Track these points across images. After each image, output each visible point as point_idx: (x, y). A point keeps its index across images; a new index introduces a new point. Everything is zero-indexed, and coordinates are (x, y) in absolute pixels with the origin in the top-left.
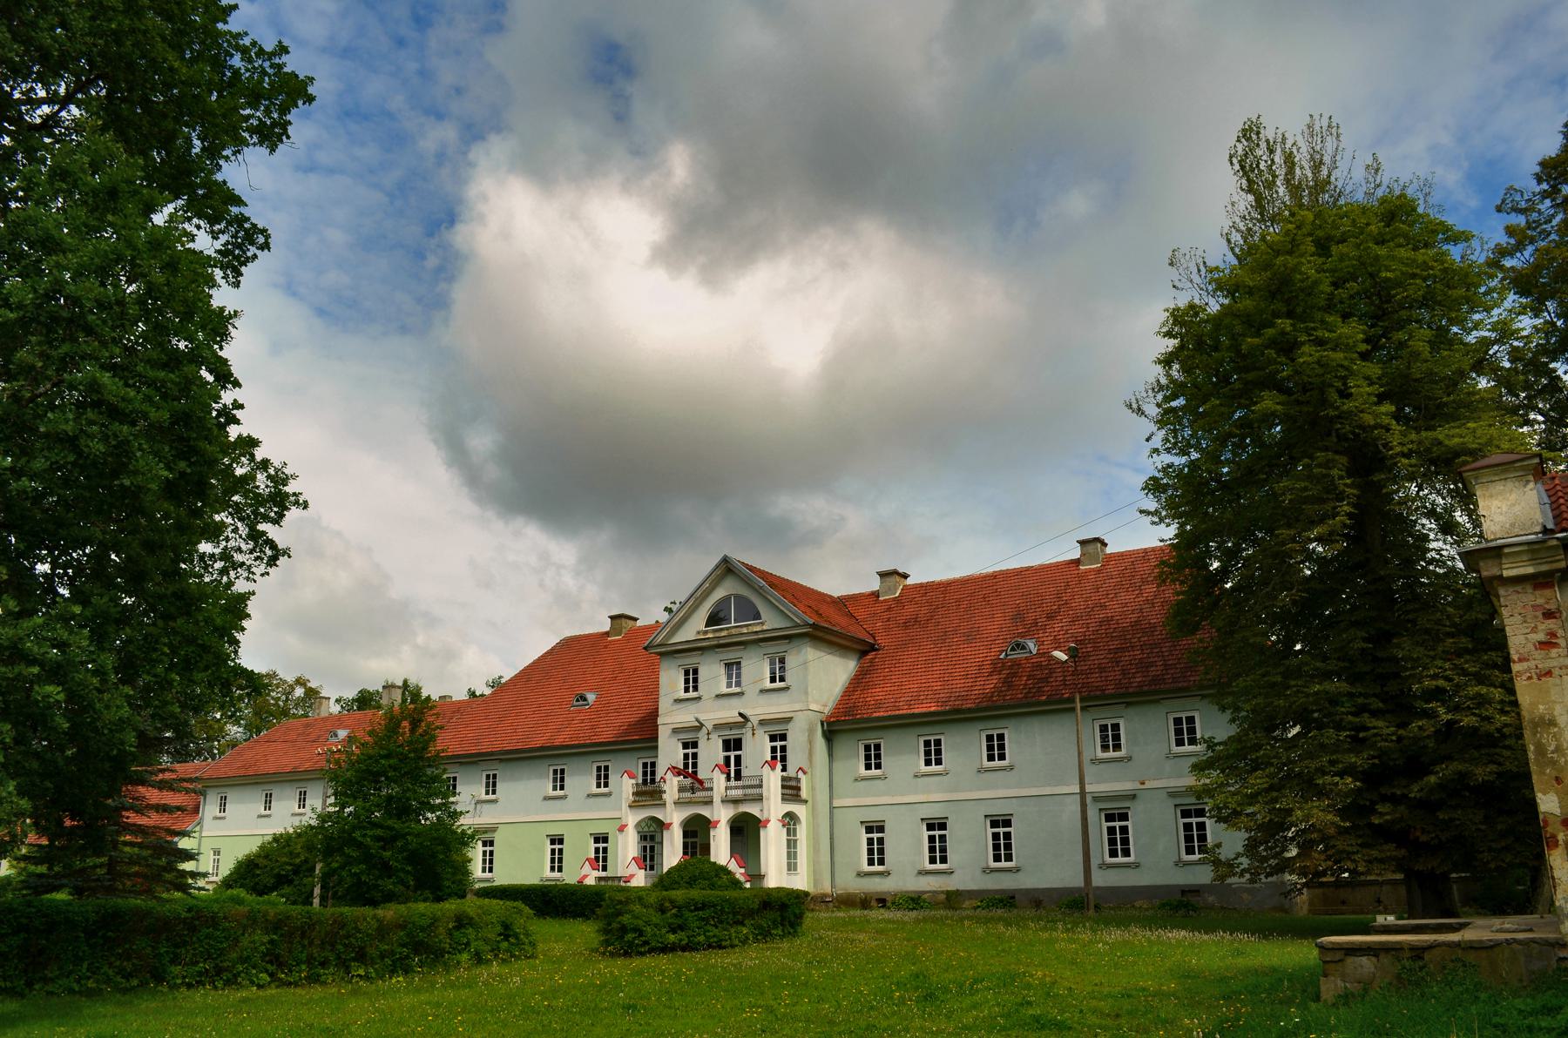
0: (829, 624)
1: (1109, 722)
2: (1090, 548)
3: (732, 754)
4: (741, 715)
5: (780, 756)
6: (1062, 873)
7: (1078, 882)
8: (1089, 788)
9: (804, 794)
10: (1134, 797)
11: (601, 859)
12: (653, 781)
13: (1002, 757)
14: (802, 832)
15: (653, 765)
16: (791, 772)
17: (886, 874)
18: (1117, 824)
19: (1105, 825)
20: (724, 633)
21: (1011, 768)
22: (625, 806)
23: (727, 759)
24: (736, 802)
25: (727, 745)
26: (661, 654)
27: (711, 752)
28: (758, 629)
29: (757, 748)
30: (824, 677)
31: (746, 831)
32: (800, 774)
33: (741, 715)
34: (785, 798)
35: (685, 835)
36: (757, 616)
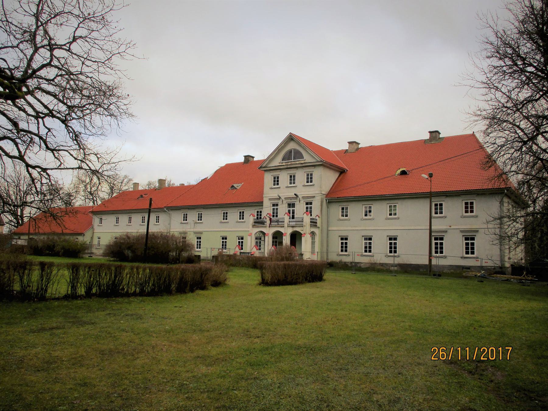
0: (327, 161)
1: (259, 210)
2: (434, 134)
3: (291, 209)
4: (295, 194)
5: (309, 211)
6: (421, 258)
7: (427, 262)
8: (433, 228)
9: (319, 224)
10: (477, 231)
11: (241, 245)
12: (261, 218)
13: (472, 211)
14: (317, 239)
15: (261, 212)
16: (313, 216)
17: (445, 257)
18: (470, 242)
19: (389, 241)
20: (290, 163)
21: (398, 218)
22: (251, 227)
23: (289, 211)
24: (293, 227)
25: (290, 205)
26: (265, 171)
27: (283, 209)
28: (303, 162)
29: (300, 209)
30: (325, 180)
31: (296, 238)
32: (317, 218)
33: (295, 194)
34: (311, 226)
35: (273, 238)
36: (302, 157)
